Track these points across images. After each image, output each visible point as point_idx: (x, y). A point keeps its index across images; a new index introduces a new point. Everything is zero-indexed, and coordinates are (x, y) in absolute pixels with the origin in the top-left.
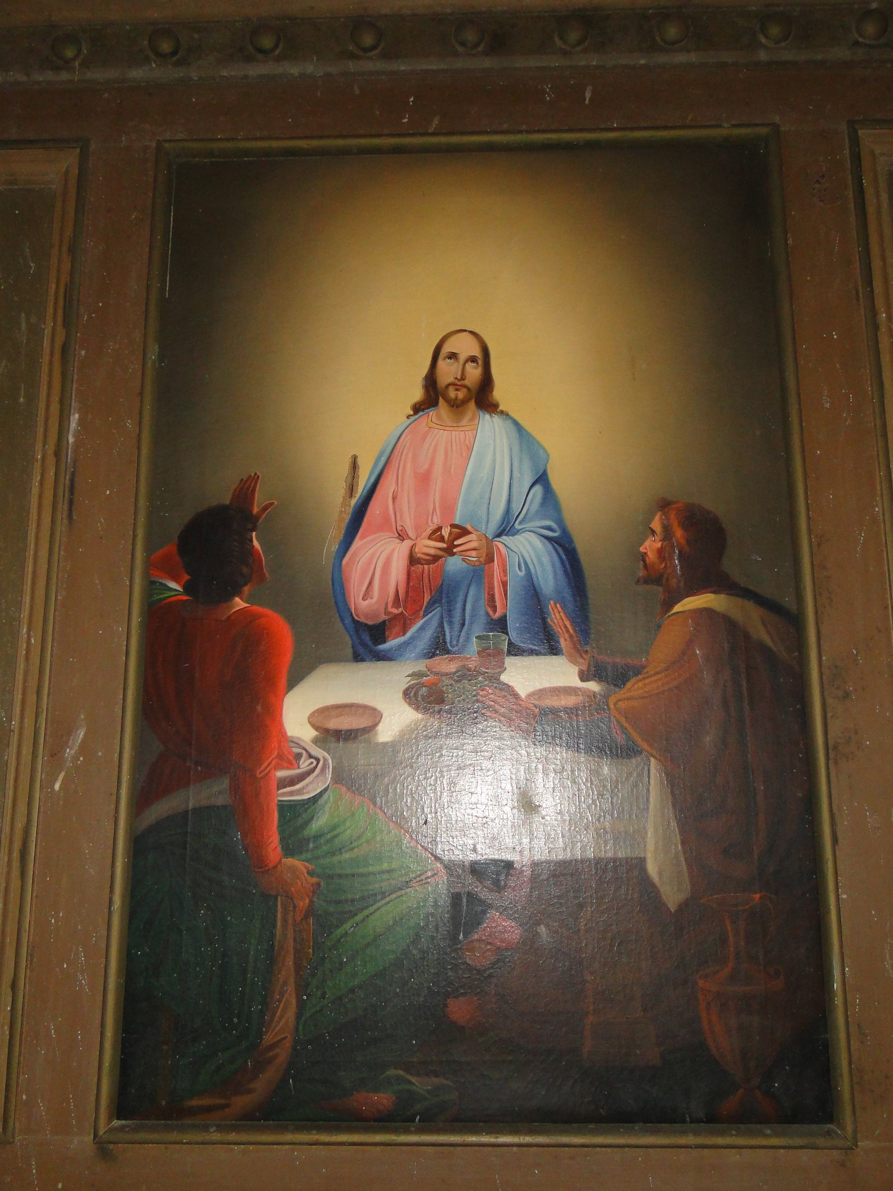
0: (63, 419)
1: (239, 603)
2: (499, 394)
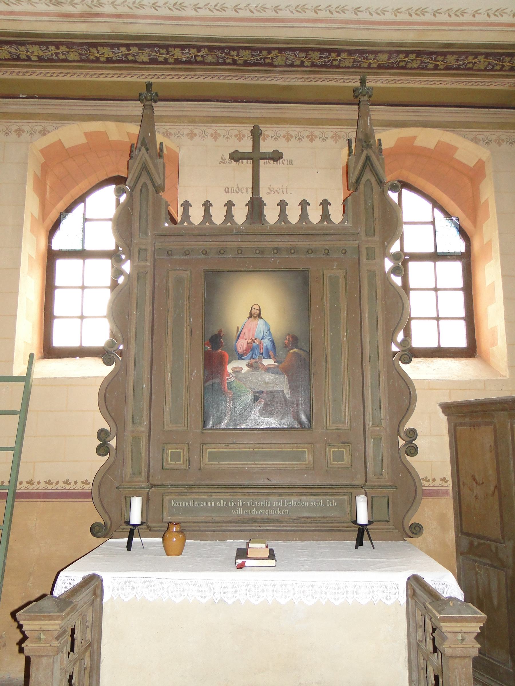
0: (190, 319)
1: (220, 350)
2: (262, 315)
